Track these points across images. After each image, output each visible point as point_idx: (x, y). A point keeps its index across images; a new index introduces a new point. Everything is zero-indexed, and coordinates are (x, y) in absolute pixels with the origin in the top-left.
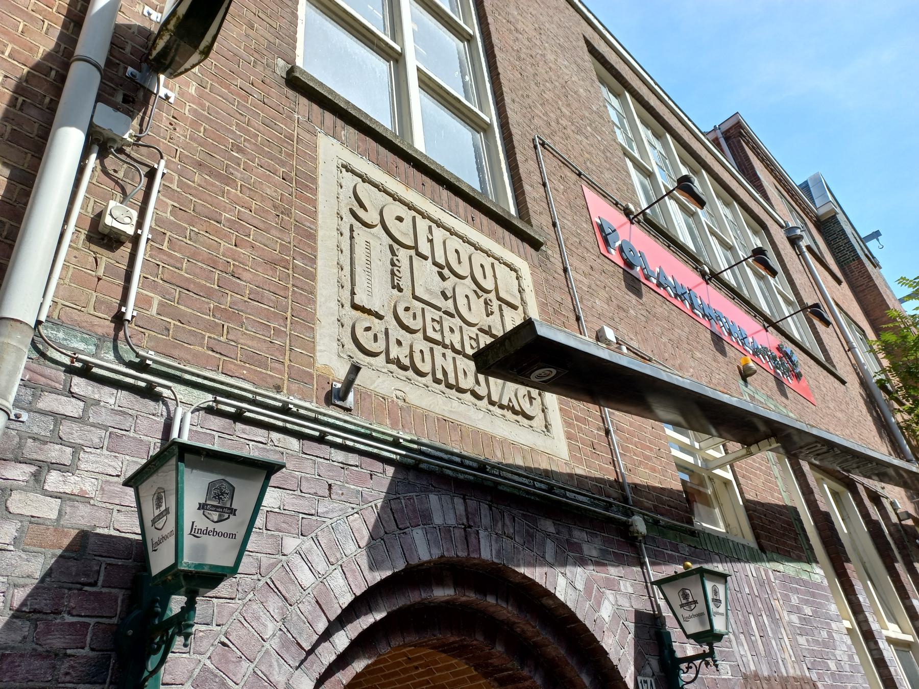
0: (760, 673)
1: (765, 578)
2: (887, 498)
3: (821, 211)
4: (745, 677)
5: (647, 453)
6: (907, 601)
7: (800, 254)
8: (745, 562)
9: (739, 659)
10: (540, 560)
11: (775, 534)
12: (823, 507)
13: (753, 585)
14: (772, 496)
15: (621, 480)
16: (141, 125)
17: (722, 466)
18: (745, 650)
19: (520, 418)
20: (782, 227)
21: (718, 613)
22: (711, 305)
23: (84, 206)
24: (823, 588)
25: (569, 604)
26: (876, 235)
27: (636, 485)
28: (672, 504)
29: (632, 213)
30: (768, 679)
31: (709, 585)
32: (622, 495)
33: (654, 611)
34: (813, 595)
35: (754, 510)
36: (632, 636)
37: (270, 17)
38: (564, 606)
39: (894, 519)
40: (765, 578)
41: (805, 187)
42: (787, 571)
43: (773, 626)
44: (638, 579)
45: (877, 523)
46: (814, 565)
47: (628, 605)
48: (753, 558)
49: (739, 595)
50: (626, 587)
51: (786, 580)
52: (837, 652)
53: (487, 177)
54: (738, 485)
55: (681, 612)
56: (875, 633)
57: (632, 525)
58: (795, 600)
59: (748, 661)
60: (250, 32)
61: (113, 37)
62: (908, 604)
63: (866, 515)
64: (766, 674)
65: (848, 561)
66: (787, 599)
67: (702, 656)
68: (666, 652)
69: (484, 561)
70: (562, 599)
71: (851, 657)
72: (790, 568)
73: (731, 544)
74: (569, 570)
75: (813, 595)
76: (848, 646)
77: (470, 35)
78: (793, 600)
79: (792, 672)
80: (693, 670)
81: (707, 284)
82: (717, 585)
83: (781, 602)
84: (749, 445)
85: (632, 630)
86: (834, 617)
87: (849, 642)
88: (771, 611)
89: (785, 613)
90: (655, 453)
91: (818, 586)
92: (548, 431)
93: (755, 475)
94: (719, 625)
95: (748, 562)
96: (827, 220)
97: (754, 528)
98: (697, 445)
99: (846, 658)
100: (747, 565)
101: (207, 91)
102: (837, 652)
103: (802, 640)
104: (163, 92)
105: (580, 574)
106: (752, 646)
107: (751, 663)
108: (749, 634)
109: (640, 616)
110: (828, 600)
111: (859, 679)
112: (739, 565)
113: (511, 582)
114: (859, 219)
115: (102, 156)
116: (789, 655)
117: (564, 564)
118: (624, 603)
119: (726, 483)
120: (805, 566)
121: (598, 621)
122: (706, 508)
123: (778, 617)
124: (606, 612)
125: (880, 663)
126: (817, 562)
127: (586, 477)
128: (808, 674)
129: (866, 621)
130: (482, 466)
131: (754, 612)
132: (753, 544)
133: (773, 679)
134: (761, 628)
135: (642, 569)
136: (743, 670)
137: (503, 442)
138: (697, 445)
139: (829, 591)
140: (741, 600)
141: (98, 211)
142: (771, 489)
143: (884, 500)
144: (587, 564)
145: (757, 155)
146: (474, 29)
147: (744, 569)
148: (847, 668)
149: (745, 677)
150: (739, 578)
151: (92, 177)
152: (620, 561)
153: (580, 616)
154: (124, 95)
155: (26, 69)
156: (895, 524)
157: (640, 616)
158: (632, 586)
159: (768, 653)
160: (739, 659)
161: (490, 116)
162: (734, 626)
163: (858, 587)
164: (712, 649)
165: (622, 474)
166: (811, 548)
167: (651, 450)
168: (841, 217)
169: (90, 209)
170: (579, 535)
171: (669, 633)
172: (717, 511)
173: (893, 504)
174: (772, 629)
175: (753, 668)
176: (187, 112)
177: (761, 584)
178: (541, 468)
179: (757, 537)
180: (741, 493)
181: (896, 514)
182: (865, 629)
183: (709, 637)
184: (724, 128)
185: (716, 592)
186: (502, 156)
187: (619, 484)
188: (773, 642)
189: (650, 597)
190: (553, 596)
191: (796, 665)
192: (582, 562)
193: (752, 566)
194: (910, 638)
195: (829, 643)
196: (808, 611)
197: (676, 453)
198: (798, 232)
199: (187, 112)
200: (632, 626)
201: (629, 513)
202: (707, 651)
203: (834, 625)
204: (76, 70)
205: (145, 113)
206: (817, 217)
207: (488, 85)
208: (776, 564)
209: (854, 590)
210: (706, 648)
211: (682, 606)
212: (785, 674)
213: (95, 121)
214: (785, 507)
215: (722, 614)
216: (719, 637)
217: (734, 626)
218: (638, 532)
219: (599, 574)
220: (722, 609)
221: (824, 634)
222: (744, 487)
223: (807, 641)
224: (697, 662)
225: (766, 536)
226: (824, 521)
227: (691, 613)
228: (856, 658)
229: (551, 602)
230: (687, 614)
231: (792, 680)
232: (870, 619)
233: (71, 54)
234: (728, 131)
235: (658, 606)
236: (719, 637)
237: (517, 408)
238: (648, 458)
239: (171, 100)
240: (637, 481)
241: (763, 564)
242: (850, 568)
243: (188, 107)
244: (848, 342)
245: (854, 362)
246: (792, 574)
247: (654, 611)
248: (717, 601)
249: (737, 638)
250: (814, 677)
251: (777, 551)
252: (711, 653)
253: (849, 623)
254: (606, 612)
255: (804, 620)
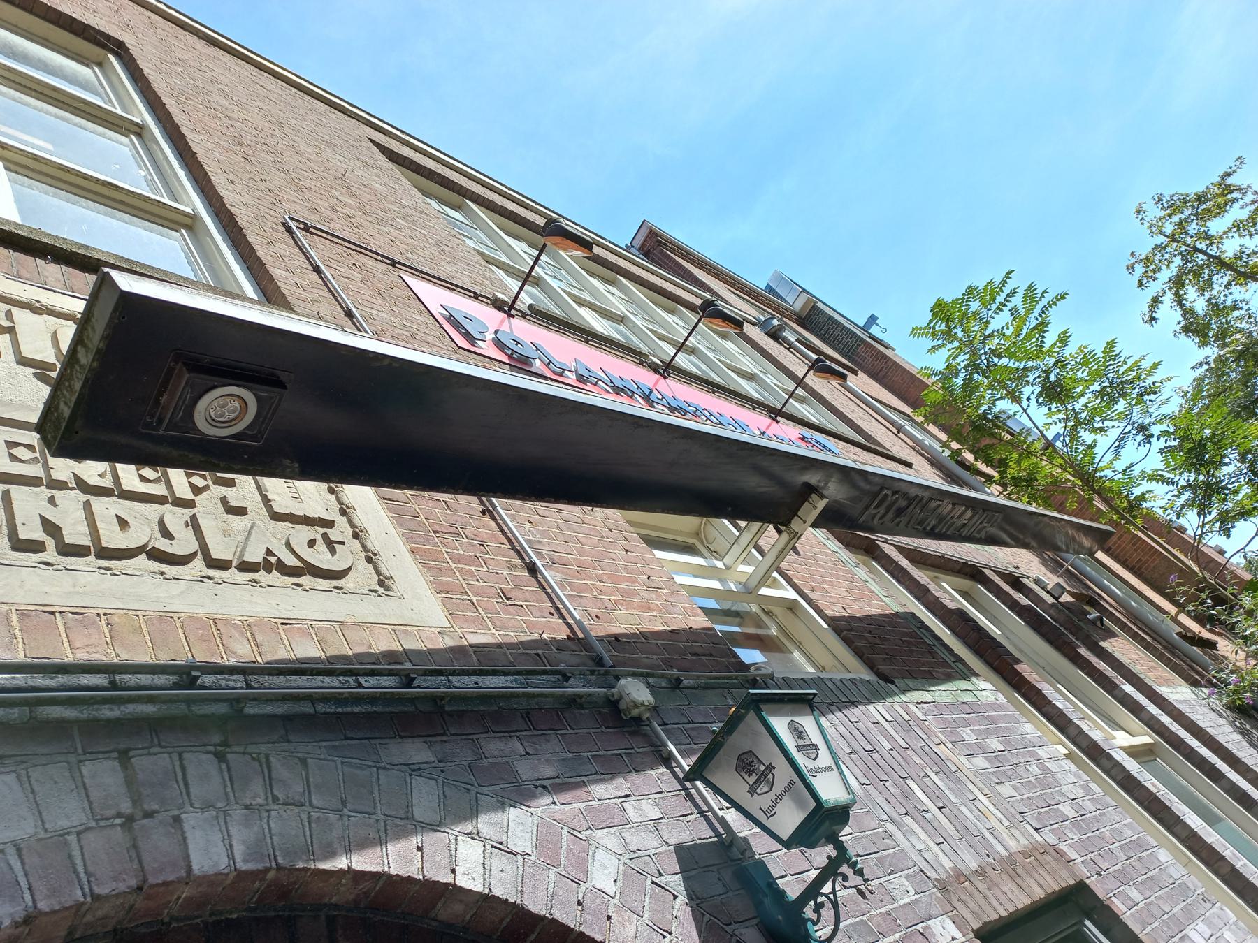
0: (963, 868)
1: (907, 718)
2: (1028, 577)
3: (798, 306)
4: (942, 886)
5: (627, 586)
6: (1116, 692)
7: (790, 347)
8: (865, 704)
9: (918, 859)
10: (406, 823)
11: (893, 655)
12: (951, 605)
13: (893, 733)
14: (870, 606)
15: (581, 635)
17: (765, 580)
18: (922, 839)
19: (306, 580)
20: (754, 324)
21: (819, 770)
22: (677, 397)
24: (1001, 707)
25: (497, 892)
26: (873, 319)
27: (617, 638)
28: (699, 651)
29: (505, 303)
30: (981, 873)
31: (780, 724)
32: (590, 657)
33: (718, 835)
34: (992, 720)
35: (852, 632)
36: (682, 899)
38: (487, 901)
39: (1050, 600)
40: (907, 718)
41: (769, 289)
42: (938, 699)
43: (952, 785)
44: (664, 787)
45: (1028, 608)
46: (974, 679)
47: (655, 843)
48: (875, 695)
49: (875, 756)
50: (641, 812)
51: (943, 712)
52: (1064, 788)
54: (810, 602)
55: (755, 804)
56: (1101, 743)
57: (621, 698)
58: (968, 735)
59: (936, 856)
62: (1120, 695)
63: (1014, 605)
64: (974, 865)
65: (1018, 662)
66: (958, 740)
67: (830, 871)
68: (768, 901)
69: (211, 880)
70: (478, 887)
71: (1086, 788)
72: (942, 693)
73: (829, 684)
74: (486, 823)
75: (992, 720)
76: (1074, 774)
77: (137, 125)
78: (966, 737)
79: (1013, 846)
80: (827, 913)
81: (665, 378)
82: (798, 719)
83: (950, 745)
84: (787, 523)
85: (680, 889)
86: (1037, 742)
87: (1073, 768)
88: (940, 764)
89: (963, 759)
90: (632, 577)
91: (993, 704)
92: (388, 588)
93: (832, 583)
94: (830, 791)
95: (869, 702)
96: (809, 315)
97: (859, 654)
98: (719, 564)
99: (1081, 793)
100: (870, 707)
102: (1064, 788)
103: (1006, 790)
105: (517, 824)
106: (932, 828)
107: (942, 856)
108: (920, 813)
109: (687, 856)
110: (1017, 721)
111: (1113, 814)
112: (855, 710)
113: (336, 907)
114: (849, 308)
116: (996, 818)
117: (473, 813)
118: (647, 842)
119: (791, 606)
120: (963, 685)
121: (587, 902)
122: (777, 655)
123: (954, 769)
124: (604, 874)
125: (1129, 784)
126: (977, 675)
127: (499, 646)
128: (1039, 839)
129: (1081, 732)
130: (186, 675)
131: (912, 773)
132: (866, 675)
133: (989, 870)
134: (935, 794)
135: (669, 767)
136: (933, 875)
137: (250, 627)
138: (719, 564)
139: (1011, 708)
140: (882, 762)
142: (863, 597)
143: (1025, 581)
144: (534, 796)
145: (692, 262)
146: (141, 114)
147: (868, 715)
148: (1090, 806)
149: (942, 886)
150: (863, 729)
152: (611, 768)
153: (536, 906)
156: (1052, 605)
157: (687, 856)
158: (655, 803)
159: (964, 830)
160: (918, 859)
161: (193, 202)
162: (887, 808)
163: (1047, 690)
164: (840, 847)
165: (579, 623)
166: (958, 659)
167: (633, 581)
168: (819, 305)
170: (496, 748)
171: (762, 864)
172: (796, 654)
173: (1037, 582)
174: (952, 790)
175: (948, 864)
177: (906, 727)
178: (375, 650)
179: (871, 666)
180: (819, 611)
181: (1048, 592)
182: (1084, 745)
183: (824, 823)
184: (638, 243)
185: (799, 733)
186: (224, 247)
187: (578, 643)
188: (963, 808)
189: (702, 813)
190: (451, 892)
191: (1014, 831)
192: (520, 794)
193: (879, 706)
194: (1146, 739)
195: (1047, 780)
196: (996, 745)
197: (680, 579)
198: (775, 322)
200: (676, 883)
201: (610, 678)
202: (834, 853)
203: (1041, 752)
206: (795, 313)
207: (181, 173)
208: (917, 693)
209: (1044, 697)
210: (830, 850)
211: (752, 791)
212: (1004, 853)
214: (896, 615)
215: (829, 769)
216: (841, 814)
217: (887, 808)
218: (636, 706)
219: (568, 807)
220: (825, 759)
221: (1034, 769)
222: (821, 604)
223: (1015, 788)
224: (827, 888)
225: (884, 660)
226: (960, 622)
227: (772, 795)
228: (1093, 785)
229: (458, 908)
230: (765, 801)
231: (1020, 858)
232: (1085, 728)
234: (643, 245)
235: (722, 821)
236: (841, 814)
237: (290, 560)
238: (633, 594)
240: (617, 629)
241: (896, 698)
242: (1025, 670)
244: (893, 423)
245: (911, 443)
246: (949, 700)
247: (718, 835)
248: (808, 748)
249: (899, 826)
250: (1052, 839)
251: (911, 675)
252: (842, 855)
253: (1060, 747)
254: (604, 874)
255: (997, 758)
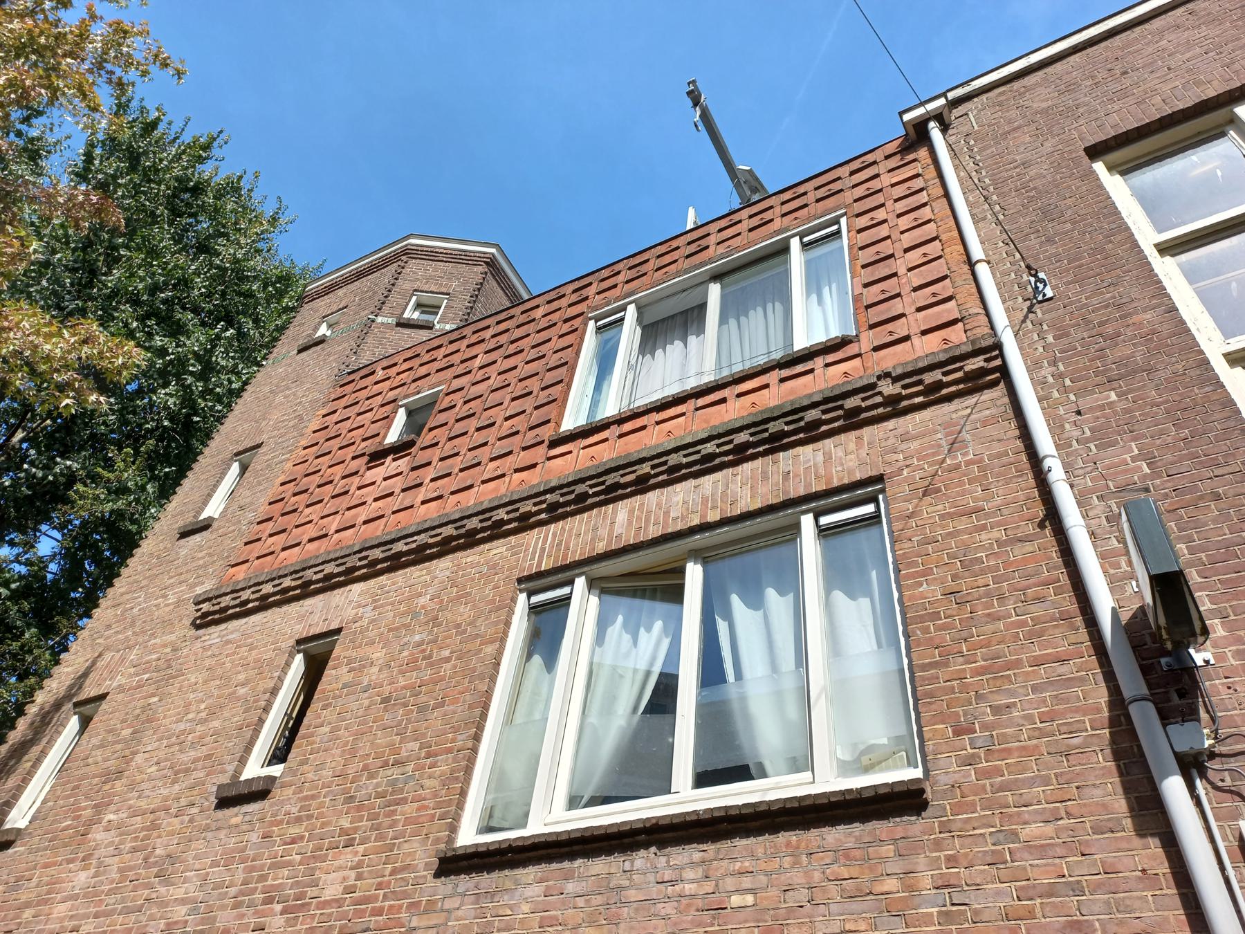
16: (1208, 712)
23: (1225, 838)
37: (1226, 464)
53: (608, 451)
60: (1222, 504)
61: (1131, 642)
101: (1232, 617)
104: (1200, 662)
115: (1203, 775)
141: (1237, 835)
151: (1210, 803)
154: (1177, 691)
155: (1107, 731)
169: (1231, 838)
176: (1233, 662)
199: (1233, 662)
204: (1133, 710)
205: (1202, 697)
213: (1177, 749)
233: (1123, 700)
239: (1212, 662)
243: (1229, 654)
